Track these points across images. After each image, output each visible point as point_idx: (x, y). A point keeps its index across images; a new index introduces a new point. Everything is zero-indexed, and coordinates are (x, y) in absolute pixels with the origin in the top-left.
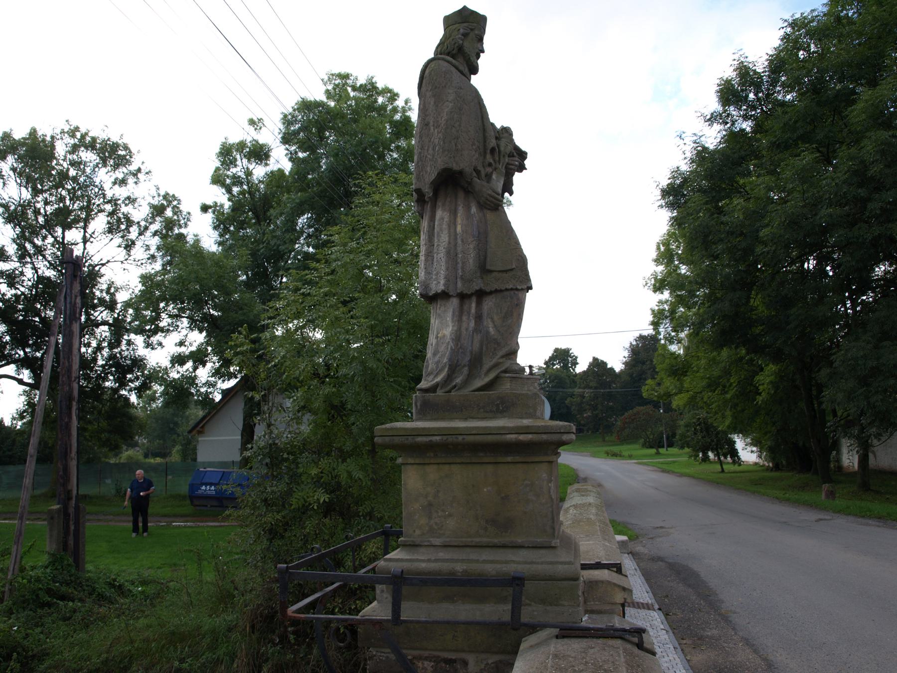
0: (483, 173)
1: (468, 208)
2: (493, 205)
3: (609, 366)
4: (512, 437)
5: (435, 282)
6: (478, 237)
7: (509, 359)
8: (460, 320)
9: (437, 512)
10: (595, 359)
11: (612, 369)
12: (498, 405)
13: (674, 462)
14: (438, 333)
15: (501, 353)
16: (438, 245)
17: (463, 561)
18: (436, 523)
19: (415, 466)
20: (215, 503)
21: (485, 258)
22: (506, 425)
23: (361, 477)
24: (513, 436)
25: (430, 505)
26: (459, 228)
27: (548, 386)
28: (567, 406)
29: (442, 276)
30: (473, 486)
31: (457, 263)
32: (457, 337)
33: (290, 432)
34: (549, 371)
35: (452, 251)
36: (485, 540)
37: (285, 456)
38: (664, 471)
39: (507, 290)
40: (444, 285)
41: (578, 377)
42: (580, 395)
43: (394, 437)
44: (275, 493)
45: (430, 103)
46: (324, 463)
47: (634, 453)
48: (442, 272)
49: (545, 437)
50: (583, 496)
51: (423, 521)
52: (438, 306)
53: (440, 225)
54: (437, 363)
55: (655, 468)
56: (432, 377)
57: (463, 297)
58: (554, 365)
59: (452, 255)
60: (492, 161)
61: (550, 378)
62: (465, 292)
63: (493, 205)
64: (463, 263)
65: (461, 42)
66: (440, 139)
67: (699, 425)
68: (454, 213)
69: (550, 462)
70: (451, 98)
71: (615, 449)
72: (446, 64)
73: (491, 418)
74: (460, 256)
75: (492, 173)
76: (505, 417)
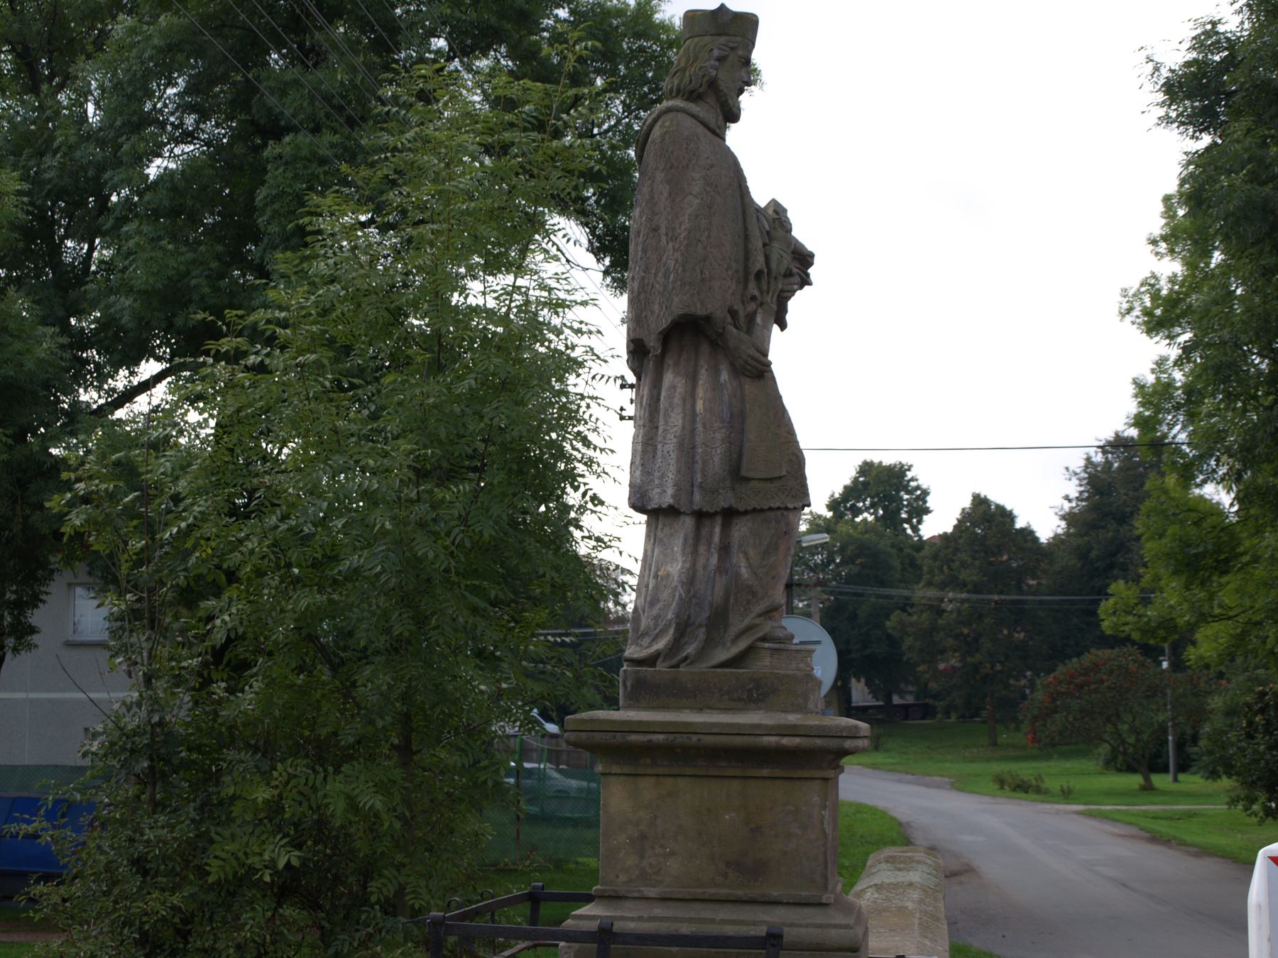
0: (742, 314)
1: (716, 372)
2: (755, 371)
3: (1019, 524)
5: (658, 490)
6: (730, 422)
7: (770, 618)
8: (695, 551)
9: (653, 848)
10: (980, 502)
11: (1028, 533)
12: (750, 690)
13: (1190, 815)
14: (658, 570)
15: (758, 609)
16: (665, 430)
17: (691, 920)
18: (651, 865)
19: (623, 778)
21: (740, 455)
22: (764, 722)
23: (379, 805)
24: (773, 739)
25: (643, 837)
26: (700, 406)
27: (837, 576)
28: (889, 637)
29: (670, 481)
30: (709, 810)
31: (694, 462)
32: (690, 580)
34: (842, 528)
35: (686, 441)
36: (723, 892)
38: (1155, 839)
39: (770, 509)
40: (674, 496)
41: (926, 552)
42: (931, 607)
43: (595, 734)
44: (165, 843)
45: (661, 193)
47: (1078, 784)
48: (670, 475)
49: (819, 742)
50: (899, 870)
52: (660, 526)
53: (670, 397)
54: (657, 618)
55: (1142, 833)
56: (646, 641)
57: (700, 516)
58: (856, 511)
59: (687, 449)
60: (756, 292)
61: (842, 550)
62: (705, 510)
63: (755, 371)
64: (705, 462)
65: (714, 73)
66: (677, 261)
67: (1262, 711)
68: (693, 379)
69: (826, 779)
70: (696, 189)
71: (1025, 770)
72: (688, 122)
73: (744, 709)
74: (700, 451)
75: (755, 313)
76: (759, 709)
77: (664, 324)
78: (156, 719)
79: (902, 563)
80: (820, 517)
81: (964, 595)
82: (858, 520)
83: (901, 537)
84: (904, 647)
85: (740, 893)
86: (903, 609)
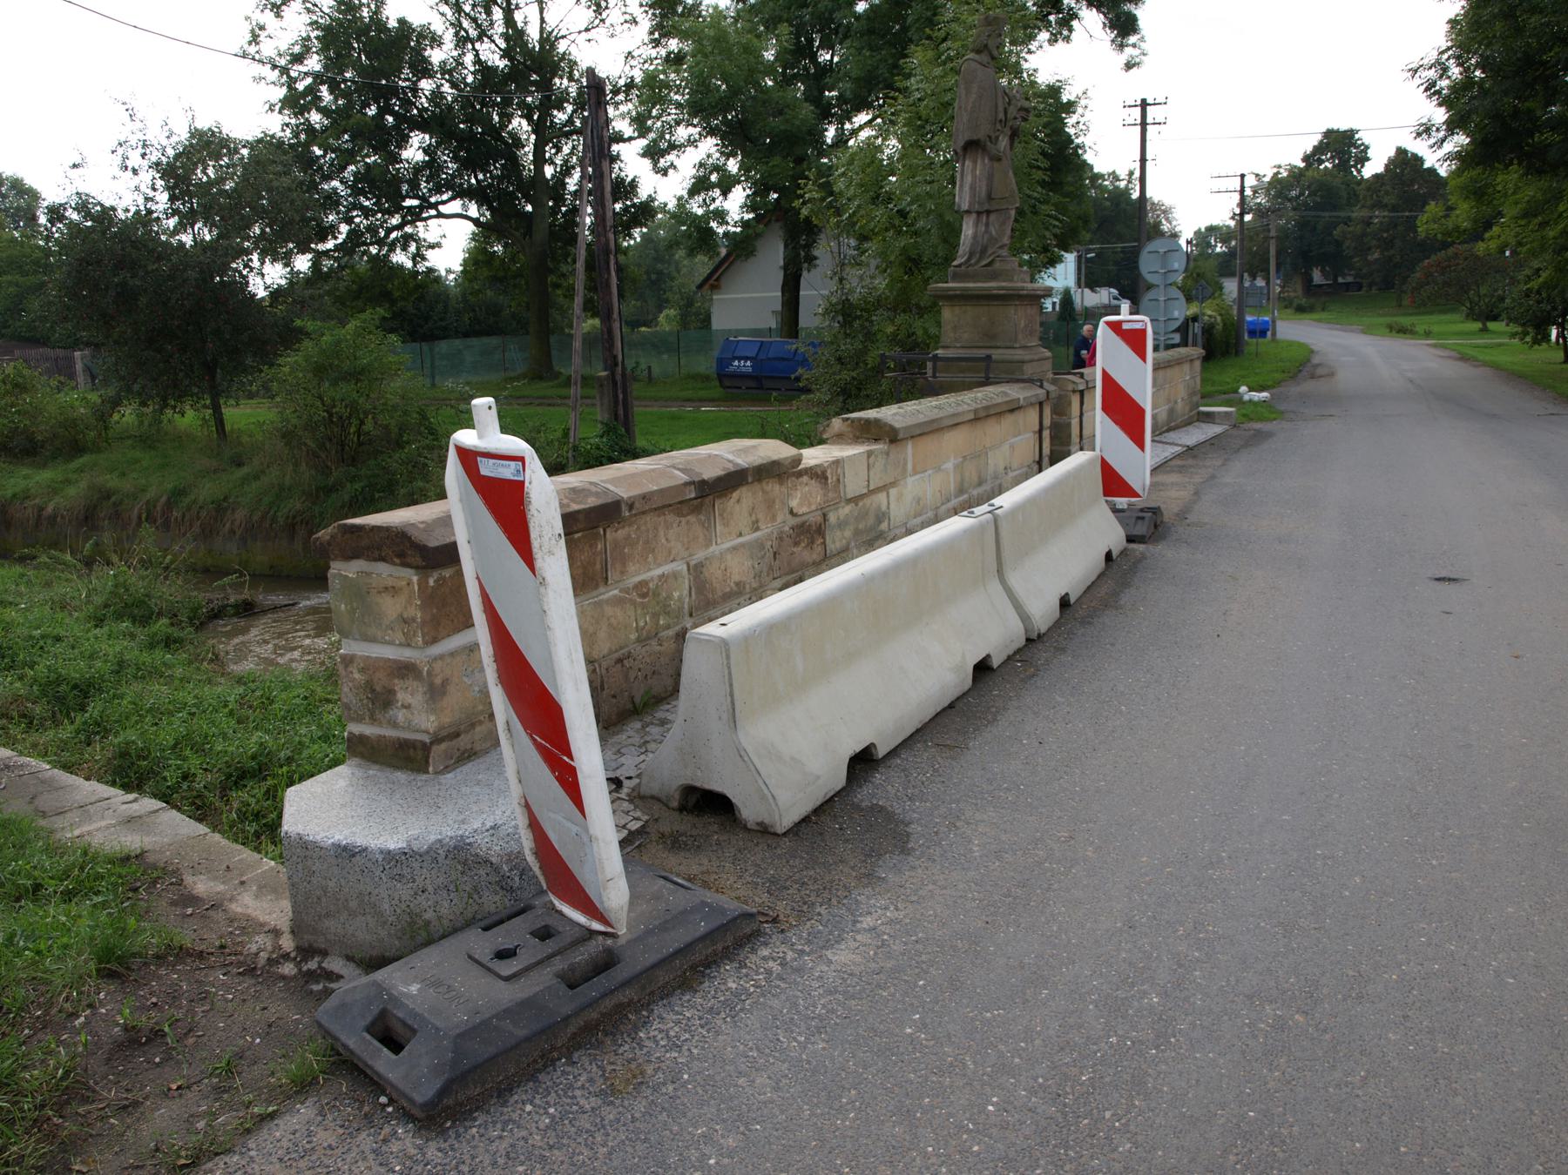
3: (1427, 165)
4: (995, 292)
20: (753, 384)
26: (978, 172)
28: (1336, 241)
32: (975, 236)
33: (863, 287)
36: (981, 344)
37: (859, 313)
41: (1363, 186)
46: (900, 319)
47: (1435, 328)
49: (1011, 292)
51: (952, 335)
57: (979, 213)
58: (1321, 162)
59: (973, 188)
61: (1309, 187)
68: (975, 162)
71: (1405, 321)
72: (973, 64)
77: (962, 144)
78: (844, 298)
79: (1349, 194)
80: (1295, 167)
81: (1386, 213)
82: (1322, 167)
83: (1349, 177)
84: (1344, 247)
85: (988, 344)
86: (1346, 224)
